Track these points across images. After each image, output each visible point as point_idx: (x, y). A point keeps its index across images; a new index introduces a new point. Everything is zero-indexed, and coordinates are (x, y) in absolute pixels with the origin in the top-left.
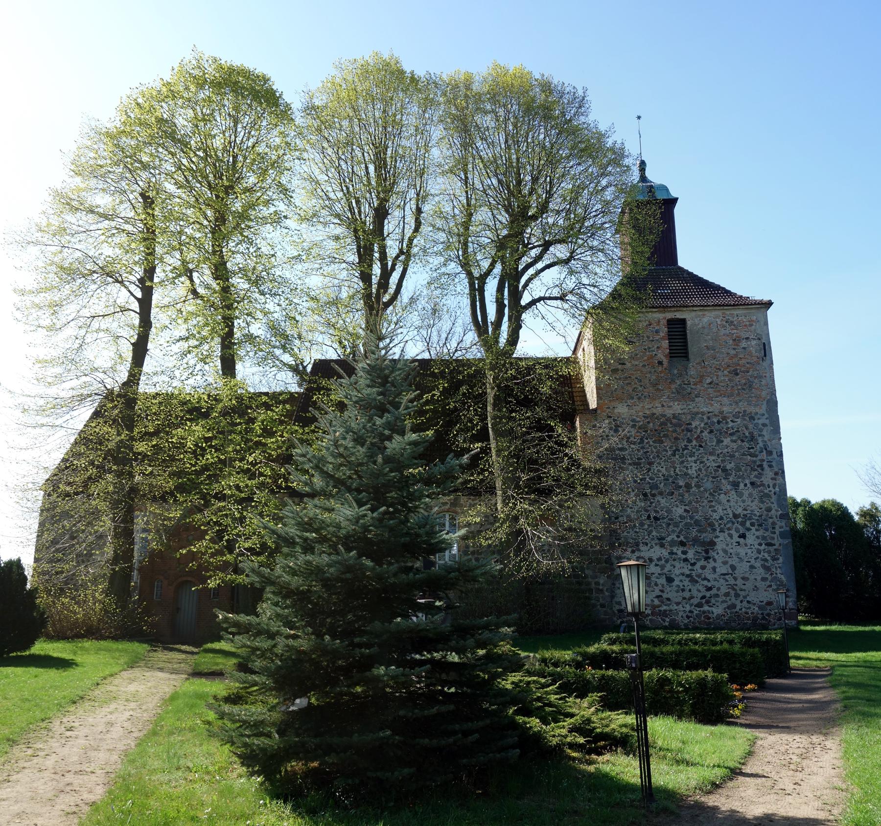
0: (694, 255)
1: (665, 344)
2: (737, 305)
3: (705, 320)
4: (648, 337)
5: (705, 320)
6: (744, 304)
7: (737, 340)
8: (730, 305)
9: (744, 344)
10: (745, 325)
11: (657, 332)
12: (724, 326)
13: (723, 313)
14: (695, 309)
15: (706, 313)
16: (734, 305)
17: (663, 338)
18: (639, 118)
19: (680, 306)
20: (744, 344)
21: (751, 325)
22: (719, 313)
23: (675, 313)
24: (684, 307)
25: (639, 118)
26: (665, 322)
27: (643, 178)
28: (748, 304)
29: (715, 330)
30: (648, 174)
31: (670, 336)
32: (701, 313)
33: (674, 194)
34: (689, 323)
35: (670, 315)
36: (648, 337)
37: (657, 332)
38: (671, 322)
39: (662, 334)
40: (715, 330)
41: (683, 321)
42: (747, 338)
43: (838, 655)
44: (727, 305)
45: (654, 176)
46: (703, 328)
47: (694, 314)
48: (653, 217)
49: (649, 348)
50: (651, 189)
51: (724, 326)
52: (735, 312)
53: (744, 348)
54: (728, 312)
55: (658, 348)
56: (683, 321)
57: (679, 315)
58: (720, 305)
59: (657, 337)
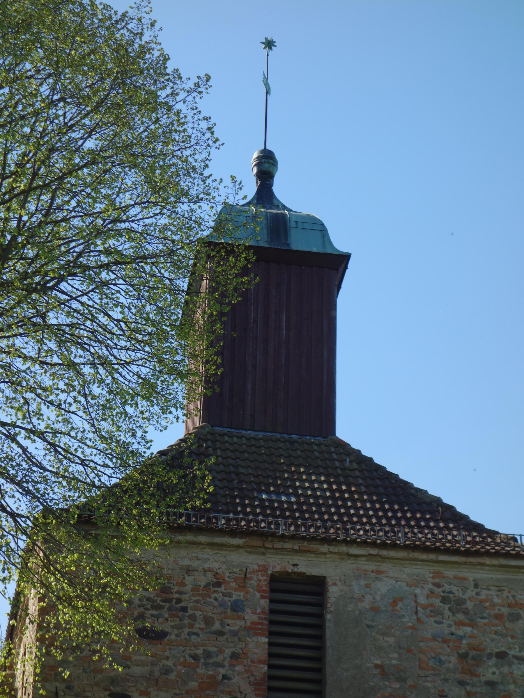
0: (369, 416)
1: (258, 645)
2: (477, 554)
3: (383, 587)
4: (208, 621)
5: (383, 587)
6: (497, 554)
7: (471, 659)
8: (457, 552)
9: (490, 671)
10: (499, 617)
11: (237, 607)
12: (436, 613)
13: (437, 574)
14: (354, 550)
15: (386, 566)
16: (467, 553)
17: (252, 629)
18: (269, 44)
19: (313, 539)
20: (490, 671)
21: (515, 618)
22: (425, 571)
23: (296, 559)
24: (324, 541)
25: (269, 44)
26: (264, 580)
27: (265, 193)
28: (507, 555)
29: (409, 620)
30: (280, 189)
31: (276, 625)
32: (370, 566)
33: (340, 243)
34: (334, 592)
35: (278, 563)
36: (208, 621)
37: (237, 607)
38: (281, 585)
39: (250, 617)
40: (409, 620)
41: (318, 585)
42: (502, 655)
43: (230, 539)
44: (447, 551)
45: (292, 193)
46: (375, 610)
47: (348, 566)
48: (274, 297)
49: (208, 655)
50: (280, 224)
51: (436, 613)
52: (471, 575)
53: (491, 684)
54: (450, 573)
55: (235, 656)
56: (318, 585)
57: (307, 566)
58: (427, 550)
59: (235, 625)
